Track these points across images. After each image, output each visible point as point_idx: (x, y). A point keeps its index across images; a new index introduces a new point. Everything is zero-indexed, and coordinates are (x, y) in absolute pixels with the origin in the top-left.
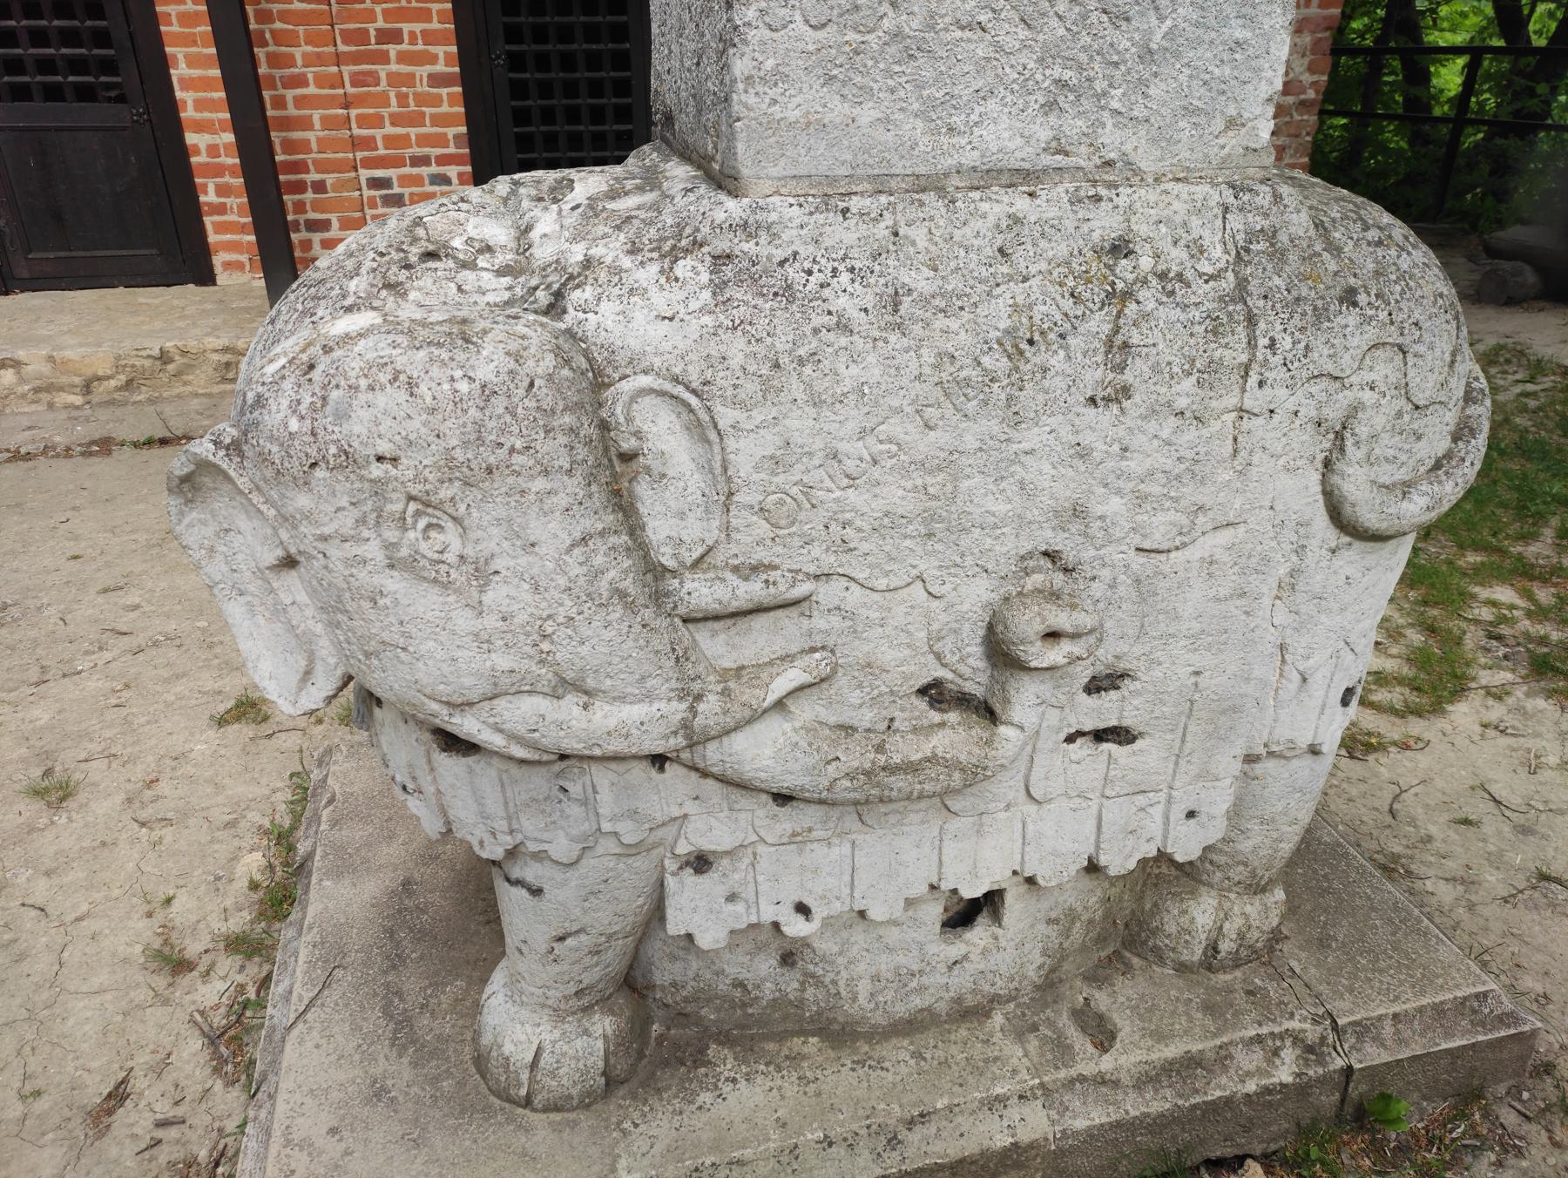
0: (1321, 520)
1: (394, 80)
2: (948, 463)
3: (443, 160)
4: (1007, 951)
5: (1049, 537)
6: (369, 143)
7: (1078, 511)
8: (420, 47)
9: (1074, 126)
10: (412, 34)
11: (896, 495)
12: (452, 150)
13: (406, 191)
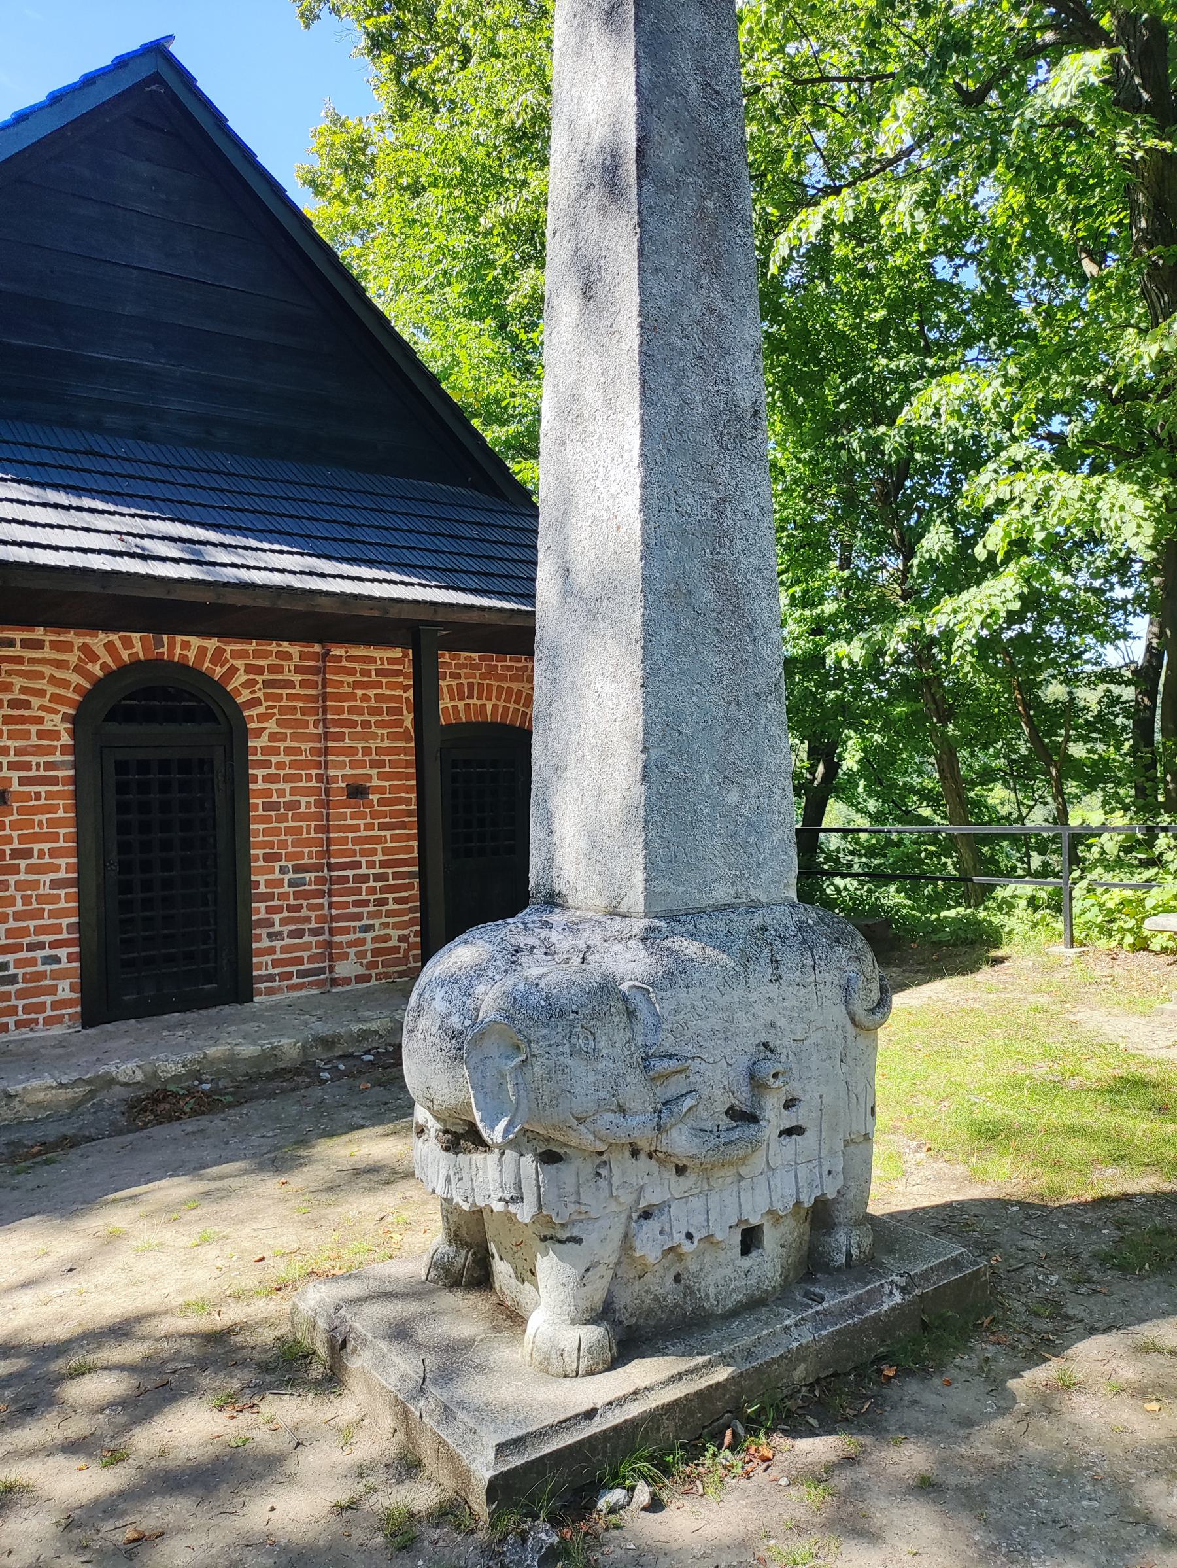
0: (849, 1026)
1: (19, 885)
3: (54, 945)
4: (769, 1265)
5: (764, 1037)
7: (772, 1025)
8: (47, 860)
9: (741, 889)
11: (713, 1022)
12: (64, 935)
13: (20, 972)
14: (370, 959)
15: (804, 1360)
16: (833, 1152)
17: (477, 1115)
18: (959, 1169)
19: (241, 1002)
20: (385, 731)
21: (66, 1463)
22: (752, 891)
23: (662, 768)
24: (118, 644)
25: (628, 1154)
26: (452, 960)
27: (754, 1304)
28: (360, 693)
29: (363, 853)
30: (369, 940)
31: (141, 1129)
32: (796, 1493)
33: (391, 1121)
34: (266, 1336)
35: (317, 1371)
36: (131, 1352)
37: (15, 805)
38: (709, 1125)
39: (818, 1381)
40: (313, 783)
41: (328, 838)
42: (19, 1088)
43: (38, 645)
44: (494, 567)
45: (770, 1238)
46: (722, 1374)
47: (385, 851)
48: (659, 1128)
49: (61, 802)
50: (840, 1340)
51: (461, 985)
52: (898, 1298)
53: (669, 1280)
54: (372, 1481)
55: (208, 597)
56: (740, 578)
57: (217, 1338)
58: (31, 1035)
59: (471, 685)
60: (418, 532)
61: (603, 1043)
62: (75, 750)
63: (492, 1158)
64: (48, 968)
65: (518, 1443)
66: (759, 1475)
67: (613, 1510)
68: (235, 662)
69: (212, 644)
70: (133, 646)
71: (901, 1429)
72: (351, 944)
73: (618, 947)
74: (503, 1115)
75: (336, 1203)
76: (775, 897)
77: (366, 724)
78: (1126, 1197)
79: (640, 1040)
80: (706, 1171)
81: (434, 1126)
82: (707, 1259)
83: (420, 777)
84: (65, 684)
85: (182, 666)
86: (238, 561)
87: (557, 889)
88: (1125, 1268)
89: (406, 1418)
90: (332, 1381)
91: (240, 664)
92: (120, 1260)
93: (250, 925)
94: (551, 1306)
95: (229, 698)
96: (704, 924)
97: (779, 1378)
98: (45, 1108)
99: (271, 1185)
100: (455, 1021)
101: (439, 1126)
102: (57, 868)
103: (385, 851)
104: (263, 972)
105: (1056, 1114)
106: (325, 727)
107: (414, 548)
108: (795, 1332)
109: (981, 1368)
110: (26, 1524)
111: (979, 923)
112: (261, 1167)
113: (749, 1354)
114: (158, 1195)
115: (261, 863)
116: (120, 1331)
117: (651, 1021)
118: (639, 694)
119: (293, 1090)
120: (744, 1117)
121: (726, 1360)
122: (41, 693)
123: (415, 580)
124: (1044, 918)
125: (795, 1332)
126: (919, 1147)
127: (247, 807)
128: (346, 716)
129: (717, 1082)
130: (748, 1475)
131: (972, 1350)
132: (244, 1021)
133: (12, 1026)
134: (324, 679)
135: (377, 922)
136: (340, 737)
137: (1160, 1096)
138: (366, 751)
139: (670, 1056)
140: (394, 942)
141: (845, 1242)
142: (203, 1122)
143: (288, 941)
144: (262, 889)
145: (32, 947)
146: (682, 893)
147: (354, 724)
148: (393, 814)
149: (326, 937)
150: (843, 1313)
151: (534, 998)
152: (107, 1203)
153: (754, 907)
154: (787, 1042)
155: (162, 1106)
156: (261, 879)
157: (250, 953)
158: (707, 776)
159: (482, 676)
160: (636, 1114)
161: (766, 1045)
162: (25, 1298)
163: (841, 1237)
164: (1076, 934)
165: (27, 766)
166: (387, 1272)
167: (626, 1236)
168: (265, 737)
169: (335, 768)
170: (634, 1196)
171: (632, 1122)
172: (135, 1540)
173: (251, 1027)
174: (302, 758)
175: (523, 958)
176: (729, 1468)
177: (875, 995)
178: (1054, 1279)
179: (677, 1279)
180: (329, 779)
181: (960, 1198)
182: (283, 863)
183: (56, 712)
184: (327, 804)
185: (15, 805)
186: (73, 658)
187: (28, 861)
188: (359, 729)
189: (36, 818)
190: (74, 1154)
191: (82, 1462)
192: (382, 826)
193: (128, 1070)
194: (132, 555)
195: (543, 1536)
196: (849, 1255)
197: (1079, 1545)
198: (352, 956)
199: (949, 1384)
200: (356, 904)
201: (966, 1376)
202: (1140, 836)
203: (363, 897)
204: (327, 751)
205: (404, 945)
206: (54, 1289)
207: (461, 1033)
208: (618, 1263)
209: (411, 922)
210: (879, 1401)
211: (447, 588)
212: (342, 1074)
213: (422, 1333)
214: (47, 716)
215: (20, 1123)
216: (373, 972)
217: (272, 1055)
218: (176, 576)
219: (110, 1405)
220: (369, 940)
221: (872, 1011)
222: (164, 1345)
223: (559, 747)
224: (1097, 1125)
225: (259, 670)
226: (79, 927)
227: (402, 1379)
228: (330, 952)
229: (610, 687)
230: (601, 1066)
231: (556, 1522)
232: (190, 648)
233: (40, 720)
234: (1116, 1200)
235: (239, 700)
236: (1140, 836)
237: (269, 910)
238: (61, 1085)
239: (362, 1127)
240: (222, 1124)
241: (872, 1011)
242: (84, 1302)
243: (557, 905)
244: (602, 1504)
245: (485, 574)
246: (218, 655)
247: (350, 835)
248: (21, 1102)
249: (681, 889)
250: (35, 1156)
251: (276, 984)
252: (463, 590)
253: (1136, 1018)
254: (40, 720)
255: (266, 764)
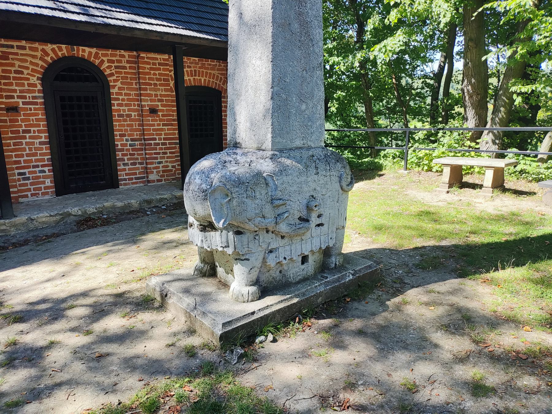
0: (340, 190)
1: (27, 143)
2: (301, 183)
3: (43, 166)
4: (310, 267)
5: (312, 193)
6: (19, 162)
8: (37, 134)
9: (305, 142)
10: (34, 131)
11: (295, 188)
12: (46, 163)
13: (31, 176)
14: (161, 173)
15: (321, 296)
16: (332, 232)
17: (213, 218)
18: (369, 239)
19: (115, 188)
20: (163, 88)
21: (71, 335)
22: (309, 143)
23: (278, 95)
24: (57, 49)
25: (265, 232)
26: (201, 165)
27: (305, 280)
28: (152, 72)
29: (157, 135)
30: (161, 167)
31: (82, 231)
32: (319, 336)
33: (175, 227)
34: (138, 294)
35: (157, 304)
36: (89, 301)
37: (22, 113)
38: (293, 223)
39: (325, 302)
40: (136, 107)
41: (143, 129)
42: (35, 217)
43: (24, 48)
44: (204, 22)
45: (311, 259)
46: (295, 300)
47: (165, 134)
48: (276, 223)
49: (40, 112)
50: (333, 290)
51: (205, 174)
52: (351, 277)
53: (278, 272)
54: (179, 337)
55: (92, 30)
56: (309, 19)
57: (120, 295)
58: (37, 199)
59: (195, 71)
60: (174, 6)
61: (258, 194)
62: (43, 91)
63: (218, 233)
64: (41, 174)
65: (230, 323)
66: (307, 331)
67: (261, 342)
68: (103, 58)
69: (94, 50)
70: (63, 51)
71: (352, 317)
72: (154, 168)
73: (262, 161)
74: (222, 218)
75: (158, 253)
76: (317, 145)
77: (155, 85)
78: (424, 247)
79: (270, 193)
80: (291, 237)
81: (196, 223)
82: (290, 265)
83: (178, 106)
84: (37, 65)
85: (83, 59)
86: (104, 15)
87: (238, 141)
88: (424, 268)
89: (190, 317)
90: (162, 307)
91: (105, 59)
92: (81, 273)
93: (116, 160)
94: (239, 281)
95: (102, 72)
96: (292, 154)
97: (313, 302)
98: (46, 224)
99: (134, 247)
100: (204, 186)
101: (198, 223)
102: (41, 137)
103: (165, 134)
104: (122, 178)
105: (402, 222)
106: (139, 85)
107: (172, 13)
108: (319, 288)
109: (378, 298)
110: (60, 353)
111: (376, 163)
112: (128, 242)
113: (304, 294)
114: (92, 252)
115: (118, 137)
116: (85, 294)
117: (274, 187)
118: (270, 65)
119: (137, 218)
120: (304, 220)
121: (296, 296)
122: (27, 68)
123: (173, 25)
124: (397, 161)
125: (319, 288)
126: (356, 233)
127: (112, 116)
128: (147, 81)
129: (296, 208)
130: (304, 331)
131: (374, 293)
132: (117, 194)
133: (29, 195)
134: (138, 66)
135: (163, 160)
136: (146, 89)
137: (434, 217)
138: (156, 95)
139: (280, 199)
140: (170, 168)
141: (334, 260)
142: (105, 228)
143: (130, 167)
144: (119, 147)
145: (34, 167)
146: (285, 142)
147: (150, 84)
148: (167, 120)
149: (145, 165)
150: (334, 282)
151: (233, 178)
152: (73, 254)
153: (309, 148)
154: (320, 195)
155: (89, 223)
156: (119, 143)
157: (117, 170)
158: (294, 99)
159: (200, 68)
160: (268, 218)
161: (312, 196)
162: (48, 285)
163: (333, 259)
164: (408, 166)
165: (25, 97)
166: (180, 273)
167: (264, 258)
168: (116, 88)
169: (144, 101)
170: (267, 246)
171: (267, 221)
172: (99, 357)
173: (120, 196)
174: (131, 97)
175: (228, 165)
176: (298, 329)
177: (349, 180)
178: (401, 272)
179: (280, 272)
180: (142, 106)
181: (369, 248)
182: (127, 138)
183: (35, 76)
184: (142, 116)
185: (22, 113)
186: (39, 54)
187: (30, 135)
188: (153, 86)
189: (31, 118)
190: (58, 239)
191: (77, 334)
192: (164, 125)
193: (75, 210)
194: (60, 10)
195: (239, 350)
196: (336, 264)
197: (409, 347)
198: (155, 172)
199: (367, 303)
200: (155, 154)
201: (373, 301)
202: (433, 132)
203: (158, 151)
204: (141, 95)
205: (174, 169)
206: (58, 282)
207: (206, 190)
208: (261, 267)
209: (176, 161)
210: (345, 308)
211: (186, 29)
212: (155, 213)
213: (194, 291)
214: (31, 78)
215: (37, 229)
216: (163, 179)
217: (129, 205)
218: (79, 20)
219: (84, 317)
220: (161, 167)
221: (348, 185)
222: (101, 298)
223: (238, 87)
224: (414, 226)
225: (113, 62)
226: (52, 159)
227: (188, 305)
228: (147, 171)
229: (258, 62)
230: (257, 202)
231: (243, 347)
232: (85, 52)
233: (28, 79)
234: (420, 248)
235: (106, 73)
236: (433, 132)
237: (123, 155)
238: (51, 216)
239: (164, 229)
240: (113, 229)
241: (348, 185)
242: (69, 286)
243: (238, 147)
244: (257, 341)
245: (201, 24)
246: (96, 56)
247: (152, 128)
248: (36, 222)
249: (284, 141)
250: (44, 240)
251: (127, 182)
252: (192, 30)
253: (427, 193)
254: (28, 79)
255: (118, 99)
